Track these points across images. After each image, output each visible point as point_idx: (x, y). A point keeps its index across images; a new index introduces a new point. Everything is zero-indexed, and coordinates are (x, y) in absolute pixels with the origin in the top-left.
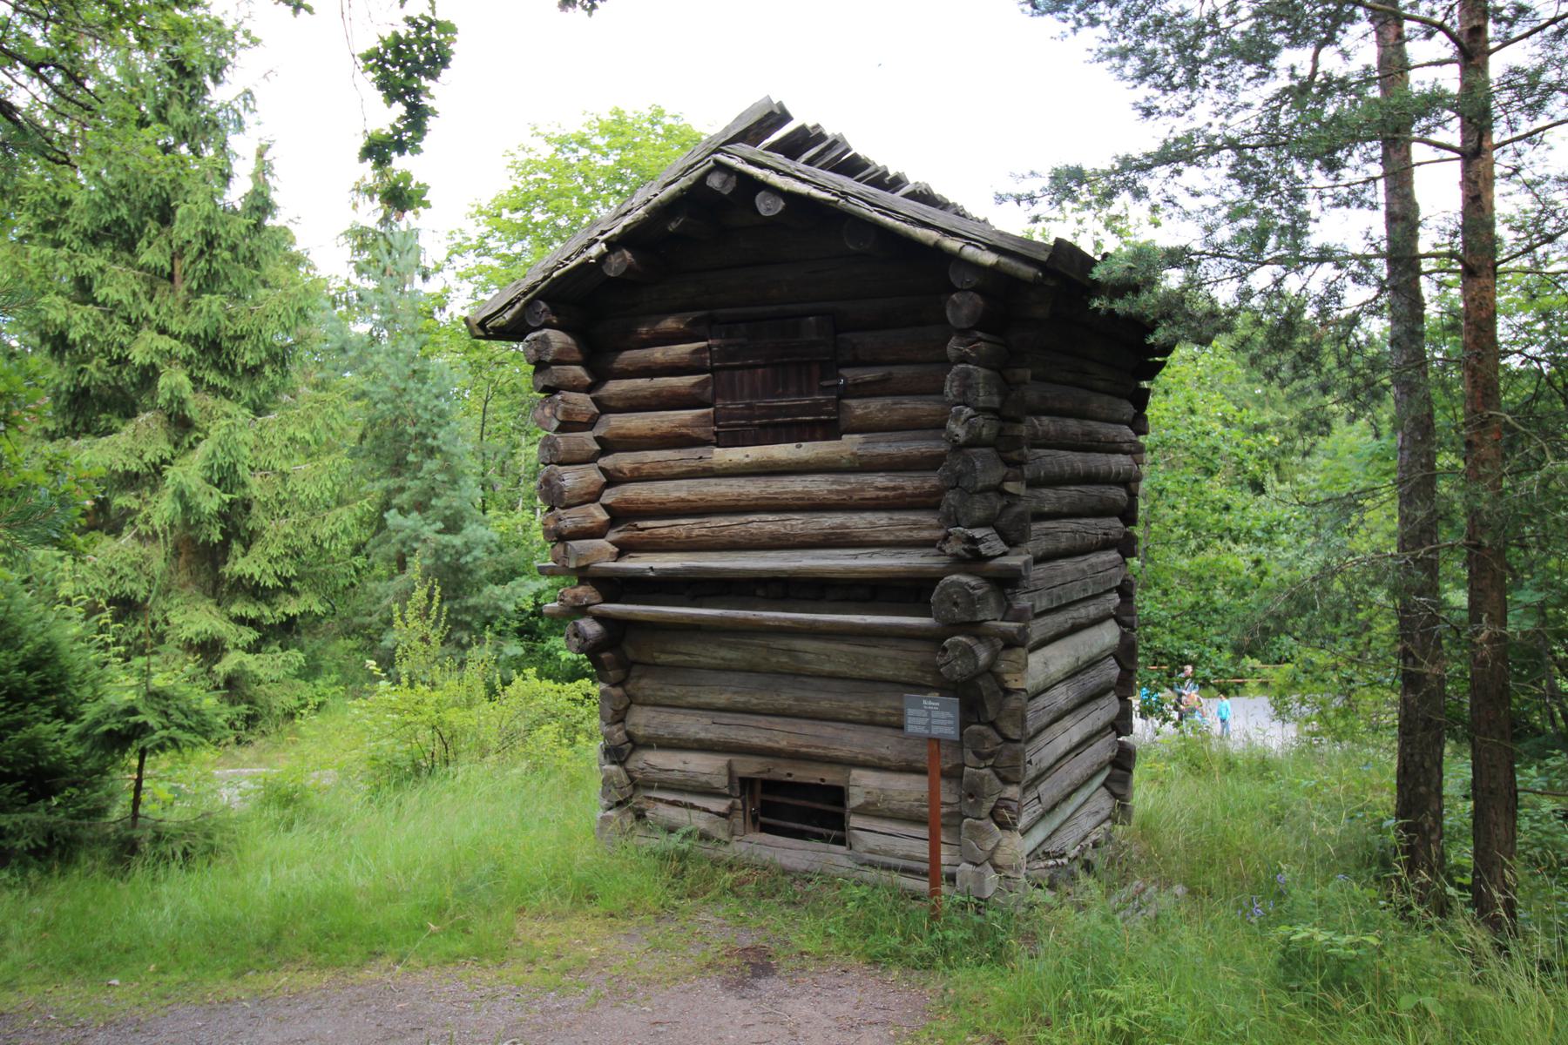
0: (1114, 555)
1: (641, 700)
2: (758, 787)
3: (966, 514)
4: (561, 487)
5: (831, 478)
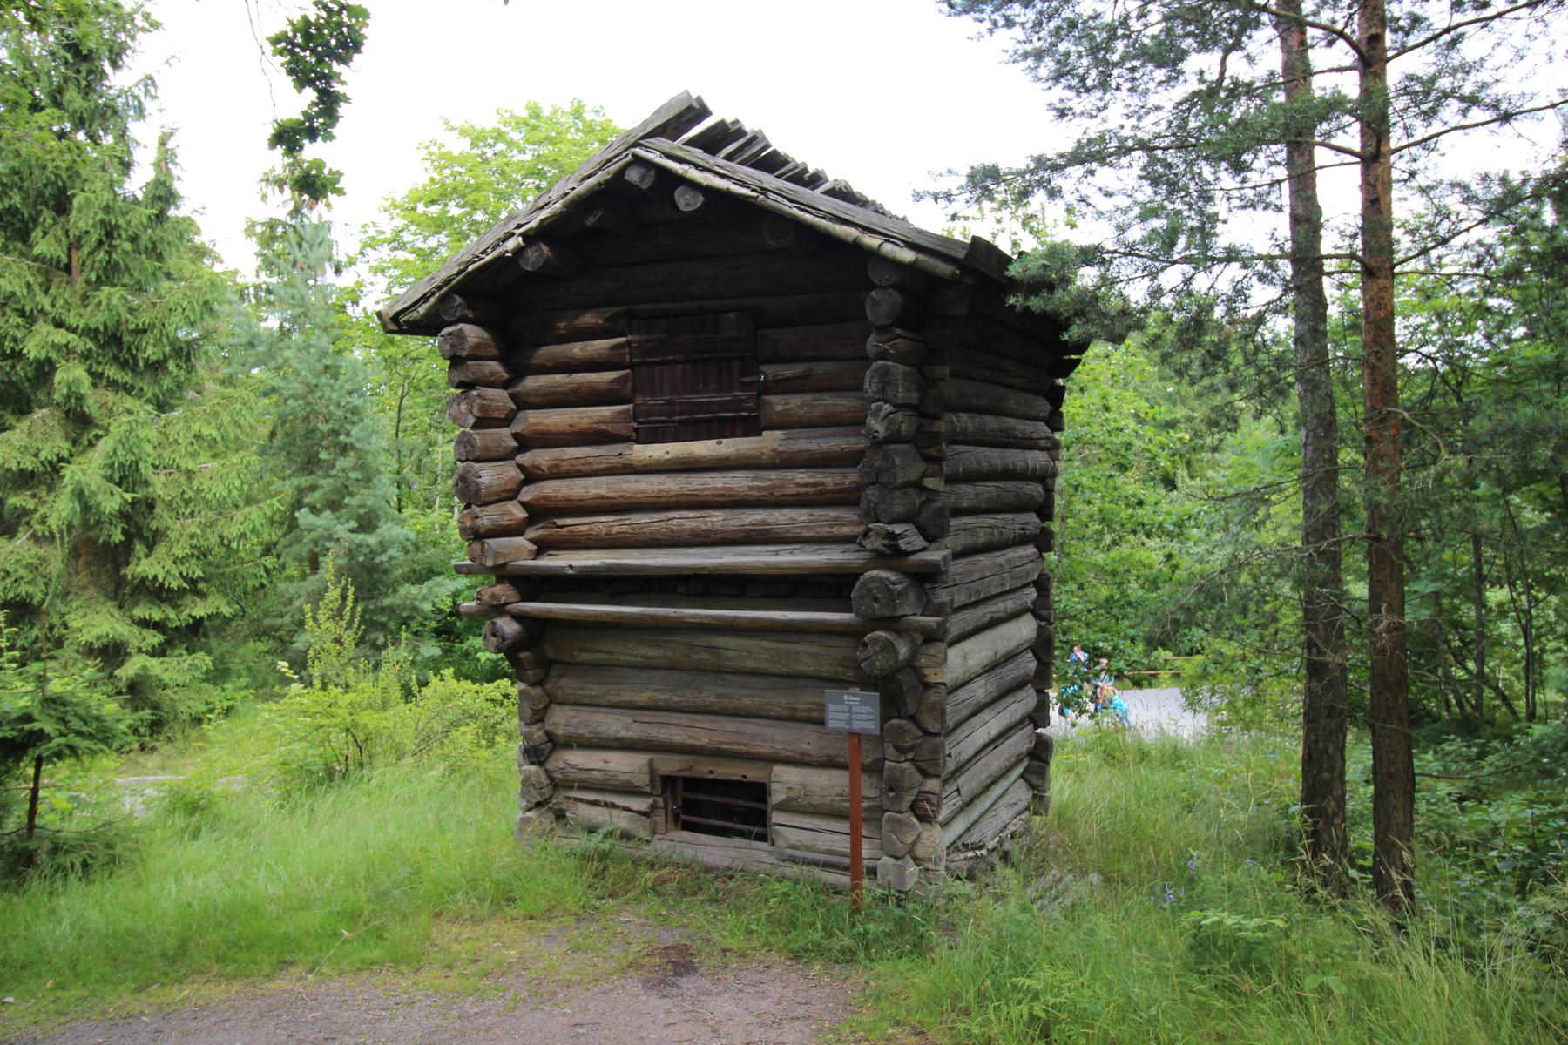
0: (1030, 550)
2: (680, 785)
4: (477, 485)
5: (751, 474)
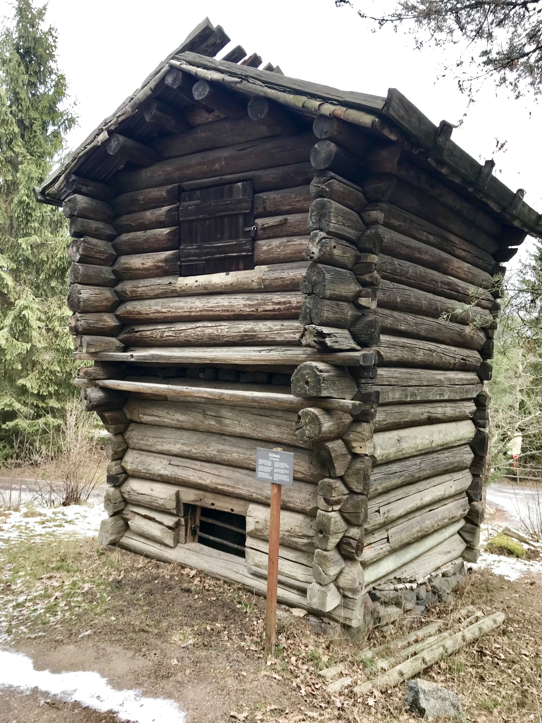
0: (472, 376)
1: (132, 447)
2: (199, 512)
3: (317, 314)
4: (79, 298)
5: (246, 296)
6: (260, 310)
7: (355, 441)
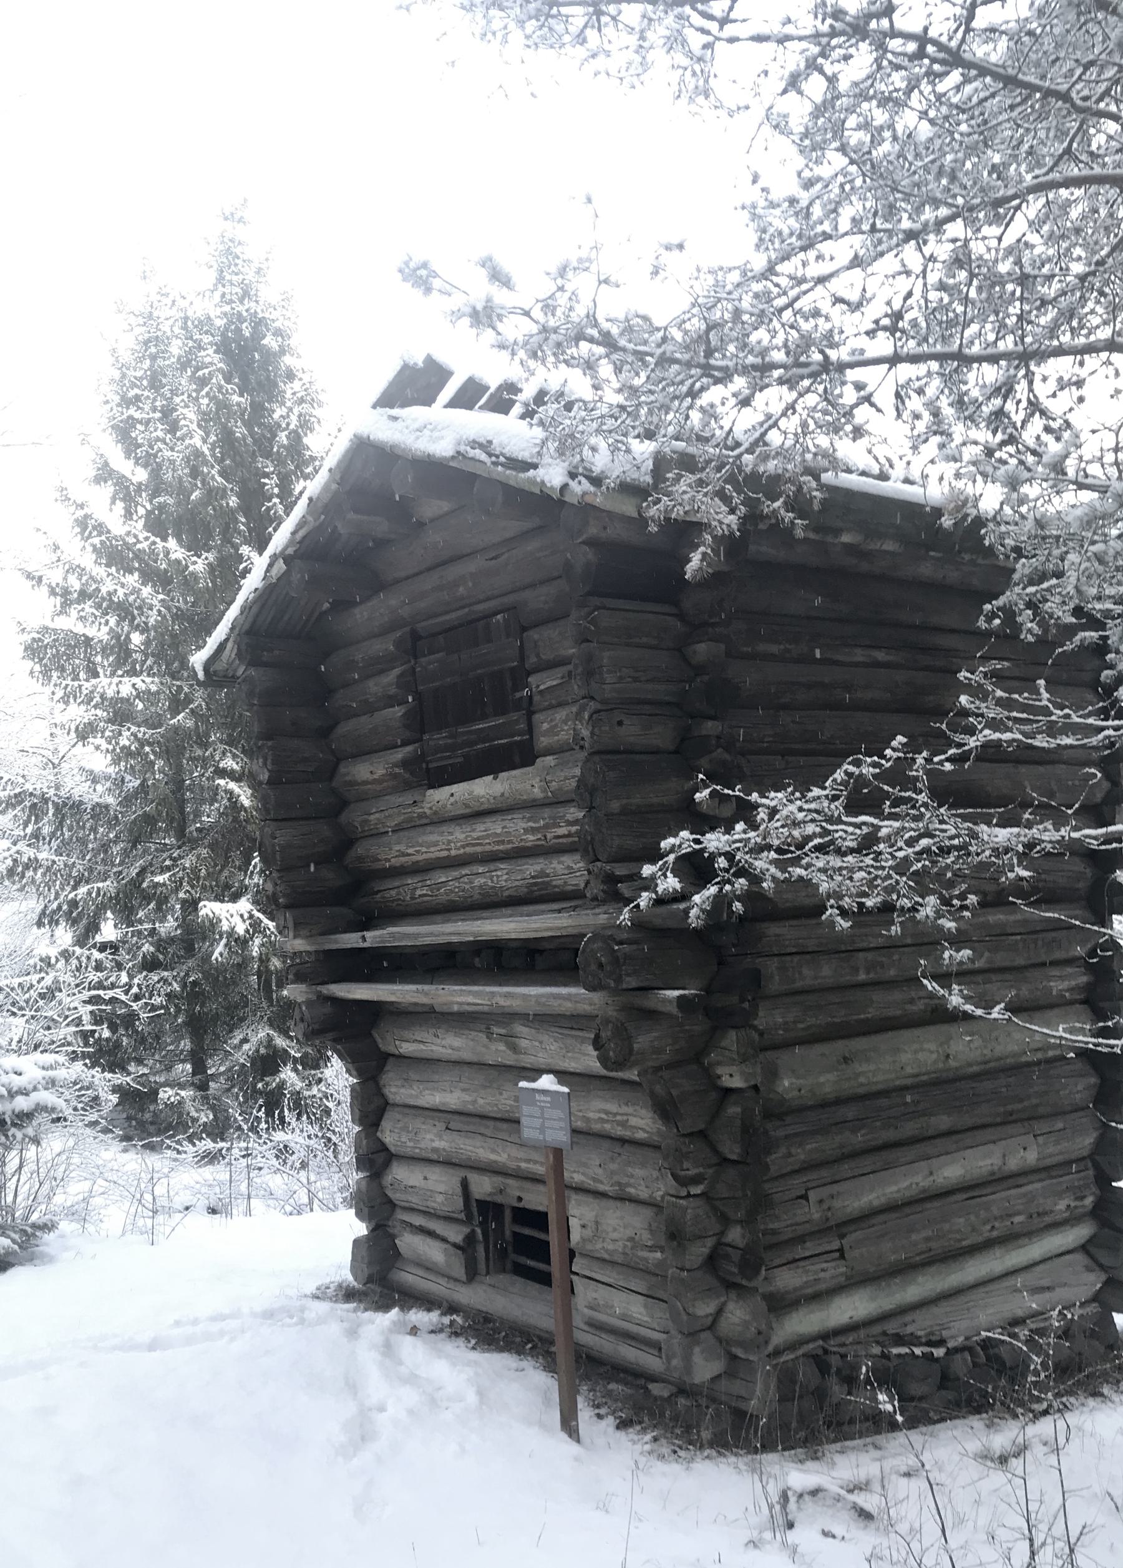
6: (549, 836)
7: (719, 1063)
